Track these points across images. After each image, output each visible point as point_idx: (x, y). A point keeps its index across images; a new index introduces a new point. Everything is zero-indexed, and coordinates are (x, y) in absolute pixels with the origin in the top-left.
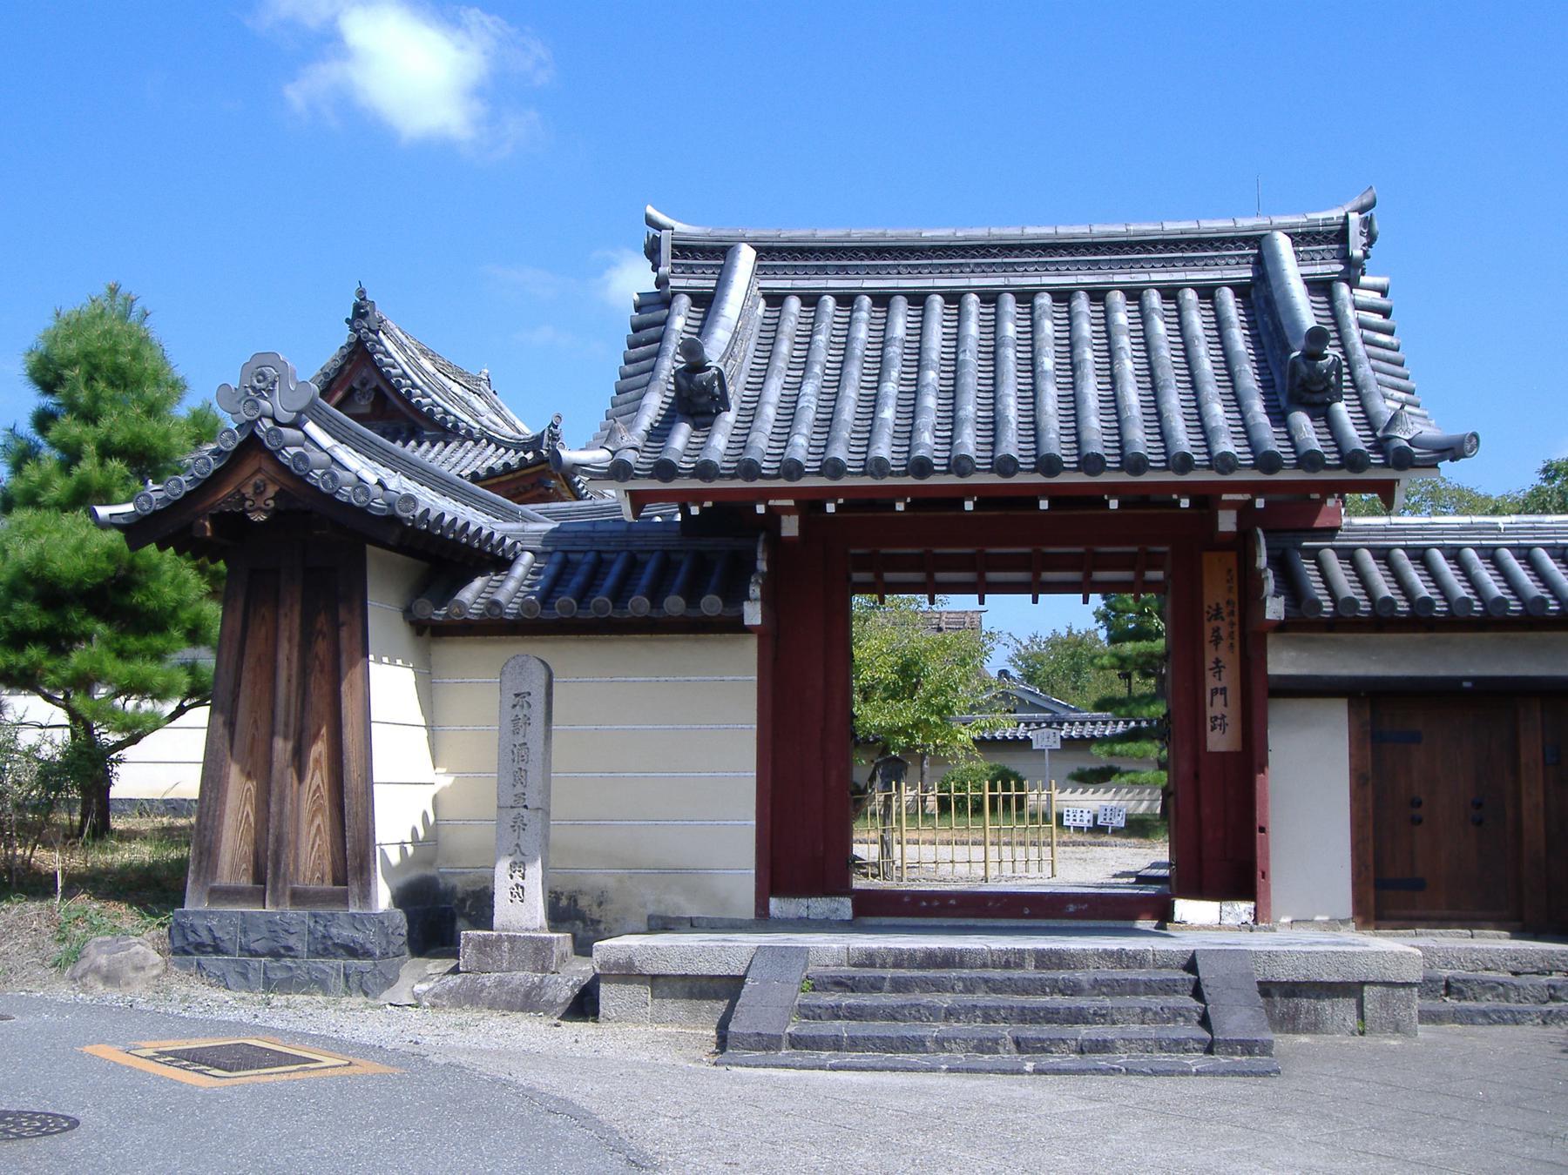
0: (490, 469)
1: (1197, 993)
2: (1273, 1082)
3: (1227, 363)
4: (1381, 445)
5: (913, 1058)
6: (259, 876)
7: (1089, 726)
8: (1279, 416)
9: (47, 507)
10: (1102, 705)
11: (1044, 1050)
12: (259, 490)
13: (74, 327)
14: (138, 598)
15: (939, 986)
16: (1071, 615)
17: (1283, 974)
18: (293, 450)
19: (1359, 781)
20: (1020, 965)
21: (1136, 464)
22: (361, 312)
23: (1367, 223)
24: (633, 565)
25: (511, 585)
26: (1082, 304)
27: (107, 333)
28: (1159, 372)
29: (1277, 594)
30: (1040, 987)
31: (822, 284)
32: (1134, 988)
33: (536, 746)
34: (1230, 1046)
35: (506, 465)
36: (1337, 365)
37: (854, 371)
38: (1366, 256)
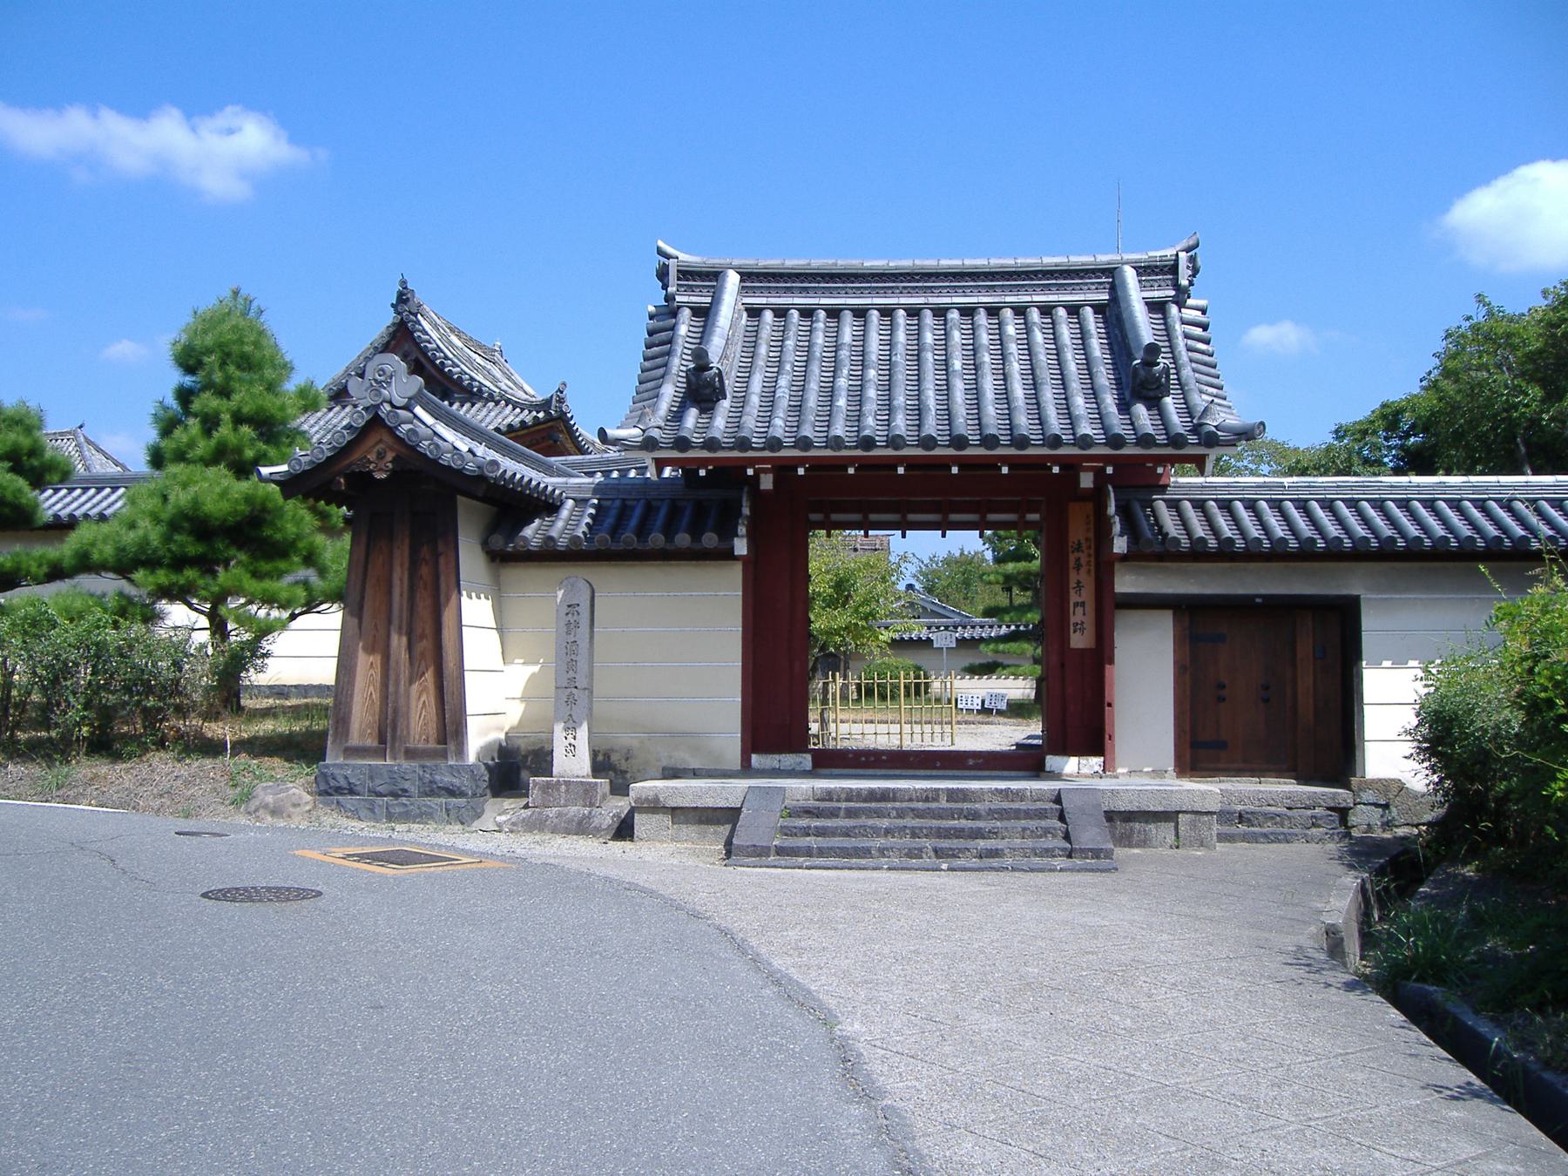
0: (510, 426)
1: (1062, 818)
2: (1114, 876)
3: (1088, 365)
4: (1196, 429)
5: (863, 862)
6: (382, 740)
7: (978, 629)
8: (1124, 407)
9: (194, 462)
10: (990, 612)
11: (954, 856)
12: (381, 456)
13: (210, 322)
14: (267, 532)
15: (879, 814)
16: (968, 542)
17: (1122, 805)
18: (406, 427)
19: (1181, 670)
20: (936, 800)
21: (1022, 442)
22: (403, 298)
23: (1192, 259)
24: (650, 510)
25: (560, 524)
26: (982, 318)
27: (235, 329)
28: (1038, 372)
29: (1121, 535)
30: (951, 815)
31: (790, 301)
32: (1017, 814)
33: (584, 645)
34: (1084, 853)
35: (523, 422)
36: (1166, 370)
37: (815, 368)
38: (1191, 283)
